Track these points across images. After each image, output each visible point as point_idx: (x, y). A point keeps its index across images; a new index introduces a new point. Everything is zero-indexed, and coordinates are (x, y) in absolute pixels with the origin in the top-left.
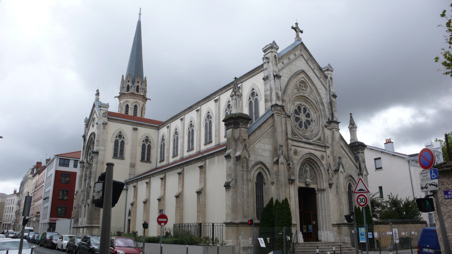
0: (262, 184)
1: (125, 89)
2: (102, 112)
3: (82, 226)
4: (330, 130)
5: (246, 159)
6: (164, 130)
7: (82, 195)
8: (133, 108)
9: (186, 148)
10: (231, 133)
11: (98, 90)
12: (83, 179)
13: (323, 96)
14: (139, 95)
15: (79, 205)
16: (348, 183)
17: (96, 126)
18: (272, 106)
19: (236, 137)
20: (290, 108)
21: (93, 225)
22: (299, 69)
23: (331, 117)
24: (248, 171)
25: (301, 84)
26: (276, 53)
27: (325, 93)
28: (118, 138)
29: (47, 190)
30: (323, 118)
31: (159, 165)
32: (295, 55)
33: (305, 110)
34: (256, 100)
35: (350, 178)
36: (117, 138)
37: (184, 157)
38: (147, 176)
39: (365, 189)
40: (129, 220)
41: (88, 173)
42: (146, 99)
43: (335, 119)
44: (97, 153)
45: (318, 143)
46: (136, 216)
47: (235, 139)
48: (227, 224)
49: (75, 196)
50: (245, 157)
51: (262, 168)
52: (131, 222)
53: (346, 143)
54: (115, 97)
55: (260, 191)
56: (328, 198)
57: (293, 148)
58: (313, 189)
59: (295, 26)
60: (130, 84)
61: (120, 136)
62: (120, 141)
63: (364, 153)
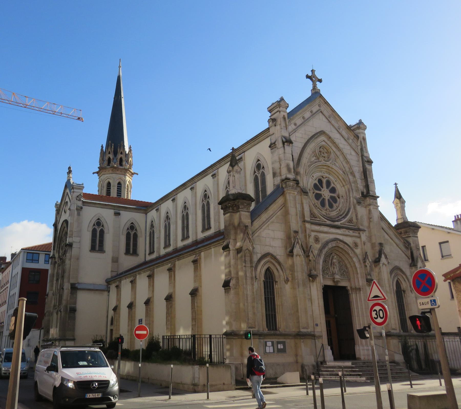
1: (106, 162)
4: (366, 207)
6: (153, 214)
9: (200, 228)
12: (55, 279)
17: (68, 212)
18: (282, 181)
20: (308, 182)
22: (318, 130)
23: (365, 191)
28: (96, 227)
29: (12, 293)
31: (149, 258)
33: (328, 183)
34: (263, 175)
38: (132, 272)
39: (380, 295)
40: (112, 330)
44: (70, 245)
47: (234, 226)
54: (94, 173)
55: (270, 292)
57: (313, 234)
58: (344, 288)
59: (310, 74)
61: (98, 223)
62: (98, 230)
63: (417, 237)
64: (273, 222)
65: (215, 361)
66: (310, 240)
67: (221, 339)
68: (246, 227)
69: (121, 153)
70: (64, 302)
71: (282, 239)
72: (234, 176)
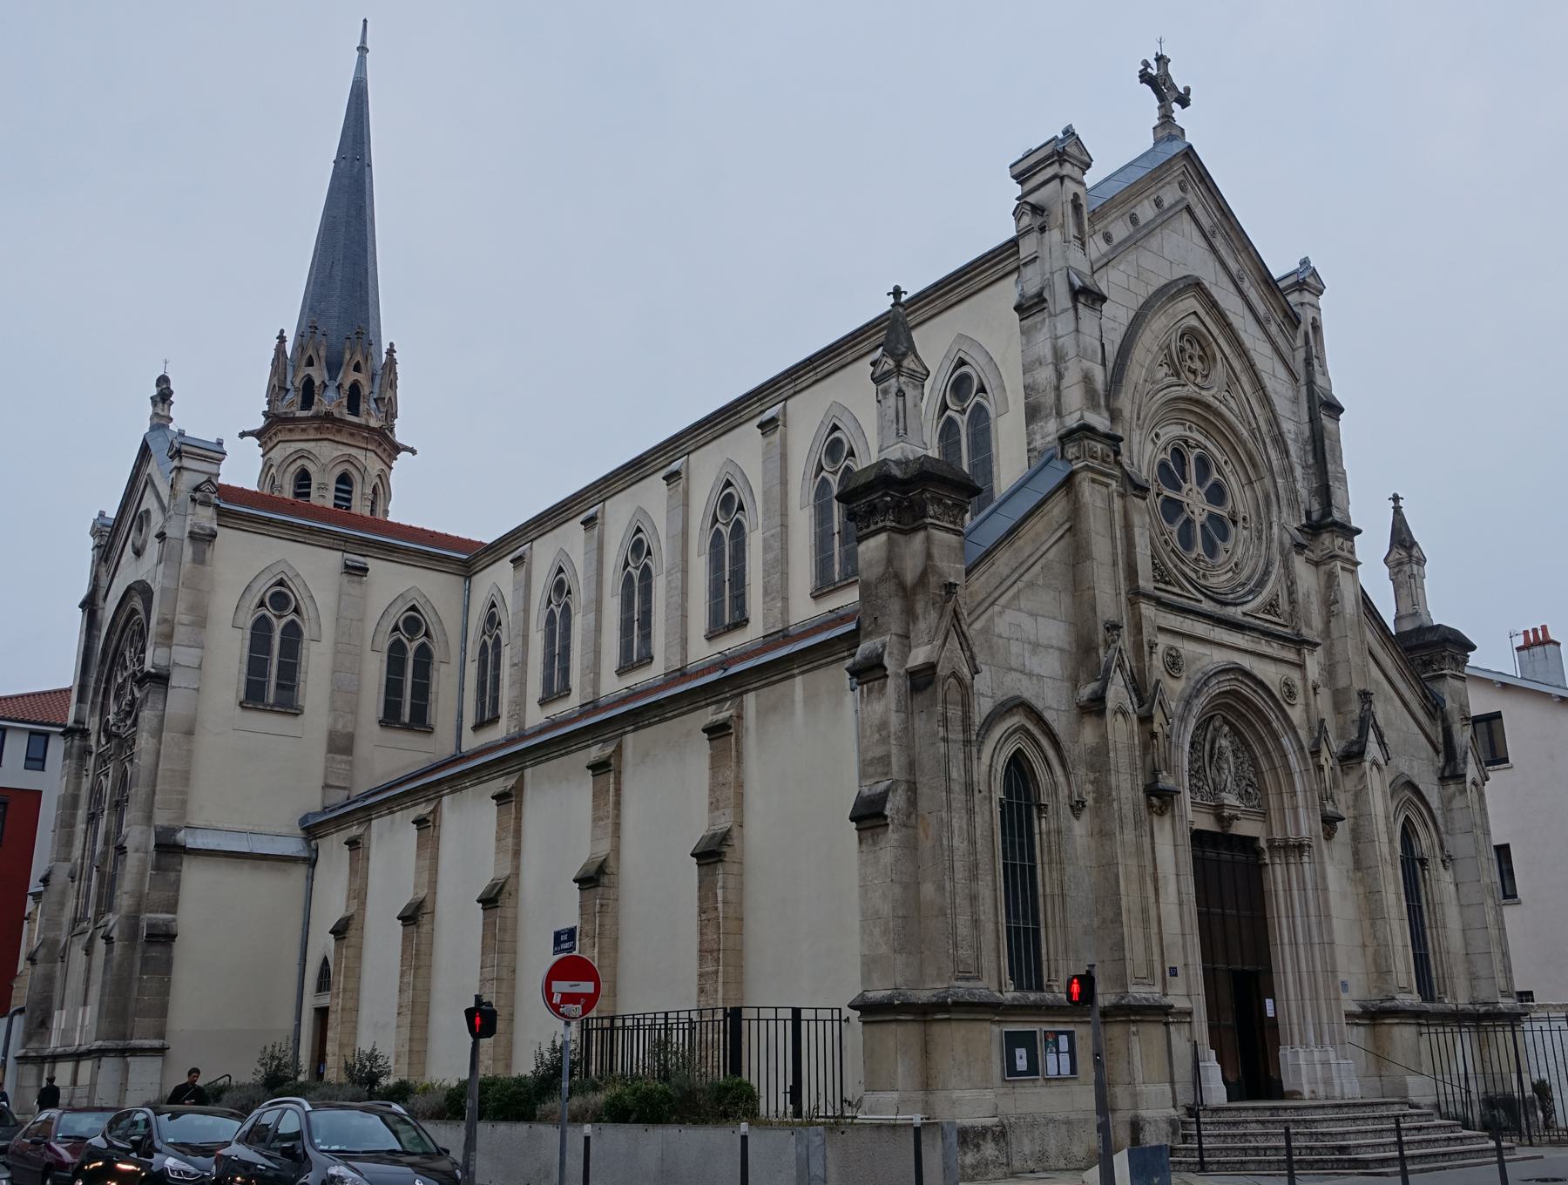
0: (1029, 808)
2: (188, 481)
3: (69, 1050)
4: (1317, 564)
5: (960, 681)
6: (499, 577)
7: (72, 893)
8: (332, 486)
10: (883, 554)
11: (163, 381)
12: (82, 813)
13: (1282, 406)
14: (359, 426)
15: (57, 942)
16: (1401, 819)
17: (153, 547)
18: (1066, 437)
19: (910, 577)
20: (1144, 456)
21: (136, 1043)
23: (1316, 506)
24: (967, 742)
25: (1187, 346)
26: (1083, 184)
27: (1290, 394)
28: (269, 613)
30: (1285, 510)
31: (471, 741)
32: (1158, 203)
33: (1203, 464)
35: (1408, 794)
36: (263, 611)
37: (603, 701)
38: (420, 793)
40: (322, 1013)
41: (107, 784)
42: (397, 449)
43: (1337, 515)
44: (160, 679)
45: (1266, 621)
46: (358, 990)
47: (902, 586)
48: (872, 1010)
49: (30, 905)
50: (954, 674)
51: (1028, 732)
52: (332, 1018)
53: (1383, 627)
54: (242, 435)
56: (1322, 887)
57: (1163, 641)
58: (1249, 843)
60: (318, 374)
64: (1031, 585)
65: (1466, 1037)
66: (1155, 662)
67: (836, 1024)
68: (950, 588)
69: (357, 368)
70: (124, 901)
71: (1061, 650)
72: (901, 393)
